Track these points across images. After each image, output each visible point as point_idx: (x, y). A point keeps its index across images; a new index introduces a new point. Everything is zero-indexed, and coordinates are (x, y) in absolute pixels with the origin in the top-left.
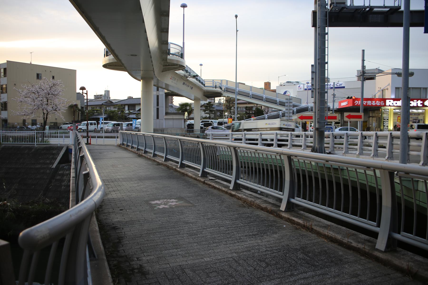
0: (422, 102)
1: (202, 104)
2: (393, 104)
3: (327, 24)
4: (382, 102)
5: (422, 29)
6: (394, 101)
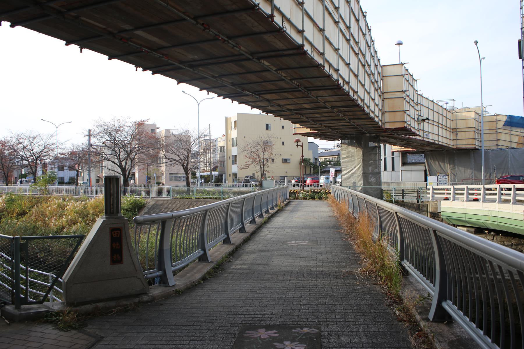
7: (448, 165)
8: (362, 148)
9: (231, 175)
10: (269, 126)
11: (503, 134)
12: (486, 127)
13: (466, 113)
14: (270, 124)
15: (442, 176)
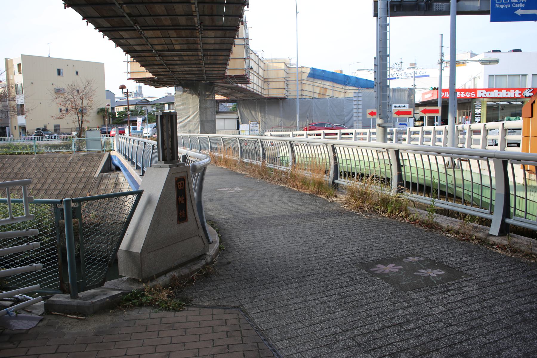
0: (520, 92)
1: (174, 31)
2: (485, 95)
3: (388, 15)
4: (473, 94)
5: (488, 17)
6: (487, 92)
7: (259, 113)
8: (199, 95)
9: (17, 128)
10: (61, 71)
11: (307, 85)
12: (292, 78)
13: (277, 64)
14: (62, 69)
15: (253, 124)
